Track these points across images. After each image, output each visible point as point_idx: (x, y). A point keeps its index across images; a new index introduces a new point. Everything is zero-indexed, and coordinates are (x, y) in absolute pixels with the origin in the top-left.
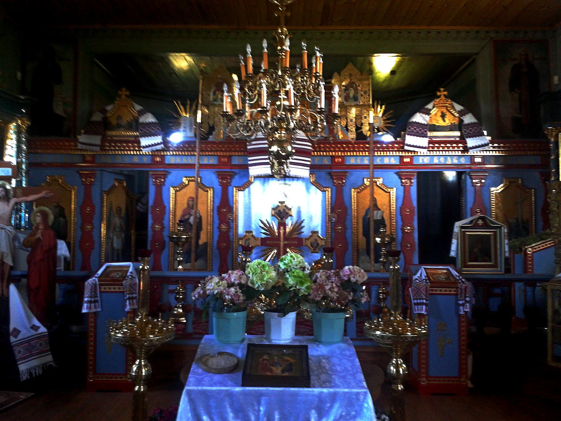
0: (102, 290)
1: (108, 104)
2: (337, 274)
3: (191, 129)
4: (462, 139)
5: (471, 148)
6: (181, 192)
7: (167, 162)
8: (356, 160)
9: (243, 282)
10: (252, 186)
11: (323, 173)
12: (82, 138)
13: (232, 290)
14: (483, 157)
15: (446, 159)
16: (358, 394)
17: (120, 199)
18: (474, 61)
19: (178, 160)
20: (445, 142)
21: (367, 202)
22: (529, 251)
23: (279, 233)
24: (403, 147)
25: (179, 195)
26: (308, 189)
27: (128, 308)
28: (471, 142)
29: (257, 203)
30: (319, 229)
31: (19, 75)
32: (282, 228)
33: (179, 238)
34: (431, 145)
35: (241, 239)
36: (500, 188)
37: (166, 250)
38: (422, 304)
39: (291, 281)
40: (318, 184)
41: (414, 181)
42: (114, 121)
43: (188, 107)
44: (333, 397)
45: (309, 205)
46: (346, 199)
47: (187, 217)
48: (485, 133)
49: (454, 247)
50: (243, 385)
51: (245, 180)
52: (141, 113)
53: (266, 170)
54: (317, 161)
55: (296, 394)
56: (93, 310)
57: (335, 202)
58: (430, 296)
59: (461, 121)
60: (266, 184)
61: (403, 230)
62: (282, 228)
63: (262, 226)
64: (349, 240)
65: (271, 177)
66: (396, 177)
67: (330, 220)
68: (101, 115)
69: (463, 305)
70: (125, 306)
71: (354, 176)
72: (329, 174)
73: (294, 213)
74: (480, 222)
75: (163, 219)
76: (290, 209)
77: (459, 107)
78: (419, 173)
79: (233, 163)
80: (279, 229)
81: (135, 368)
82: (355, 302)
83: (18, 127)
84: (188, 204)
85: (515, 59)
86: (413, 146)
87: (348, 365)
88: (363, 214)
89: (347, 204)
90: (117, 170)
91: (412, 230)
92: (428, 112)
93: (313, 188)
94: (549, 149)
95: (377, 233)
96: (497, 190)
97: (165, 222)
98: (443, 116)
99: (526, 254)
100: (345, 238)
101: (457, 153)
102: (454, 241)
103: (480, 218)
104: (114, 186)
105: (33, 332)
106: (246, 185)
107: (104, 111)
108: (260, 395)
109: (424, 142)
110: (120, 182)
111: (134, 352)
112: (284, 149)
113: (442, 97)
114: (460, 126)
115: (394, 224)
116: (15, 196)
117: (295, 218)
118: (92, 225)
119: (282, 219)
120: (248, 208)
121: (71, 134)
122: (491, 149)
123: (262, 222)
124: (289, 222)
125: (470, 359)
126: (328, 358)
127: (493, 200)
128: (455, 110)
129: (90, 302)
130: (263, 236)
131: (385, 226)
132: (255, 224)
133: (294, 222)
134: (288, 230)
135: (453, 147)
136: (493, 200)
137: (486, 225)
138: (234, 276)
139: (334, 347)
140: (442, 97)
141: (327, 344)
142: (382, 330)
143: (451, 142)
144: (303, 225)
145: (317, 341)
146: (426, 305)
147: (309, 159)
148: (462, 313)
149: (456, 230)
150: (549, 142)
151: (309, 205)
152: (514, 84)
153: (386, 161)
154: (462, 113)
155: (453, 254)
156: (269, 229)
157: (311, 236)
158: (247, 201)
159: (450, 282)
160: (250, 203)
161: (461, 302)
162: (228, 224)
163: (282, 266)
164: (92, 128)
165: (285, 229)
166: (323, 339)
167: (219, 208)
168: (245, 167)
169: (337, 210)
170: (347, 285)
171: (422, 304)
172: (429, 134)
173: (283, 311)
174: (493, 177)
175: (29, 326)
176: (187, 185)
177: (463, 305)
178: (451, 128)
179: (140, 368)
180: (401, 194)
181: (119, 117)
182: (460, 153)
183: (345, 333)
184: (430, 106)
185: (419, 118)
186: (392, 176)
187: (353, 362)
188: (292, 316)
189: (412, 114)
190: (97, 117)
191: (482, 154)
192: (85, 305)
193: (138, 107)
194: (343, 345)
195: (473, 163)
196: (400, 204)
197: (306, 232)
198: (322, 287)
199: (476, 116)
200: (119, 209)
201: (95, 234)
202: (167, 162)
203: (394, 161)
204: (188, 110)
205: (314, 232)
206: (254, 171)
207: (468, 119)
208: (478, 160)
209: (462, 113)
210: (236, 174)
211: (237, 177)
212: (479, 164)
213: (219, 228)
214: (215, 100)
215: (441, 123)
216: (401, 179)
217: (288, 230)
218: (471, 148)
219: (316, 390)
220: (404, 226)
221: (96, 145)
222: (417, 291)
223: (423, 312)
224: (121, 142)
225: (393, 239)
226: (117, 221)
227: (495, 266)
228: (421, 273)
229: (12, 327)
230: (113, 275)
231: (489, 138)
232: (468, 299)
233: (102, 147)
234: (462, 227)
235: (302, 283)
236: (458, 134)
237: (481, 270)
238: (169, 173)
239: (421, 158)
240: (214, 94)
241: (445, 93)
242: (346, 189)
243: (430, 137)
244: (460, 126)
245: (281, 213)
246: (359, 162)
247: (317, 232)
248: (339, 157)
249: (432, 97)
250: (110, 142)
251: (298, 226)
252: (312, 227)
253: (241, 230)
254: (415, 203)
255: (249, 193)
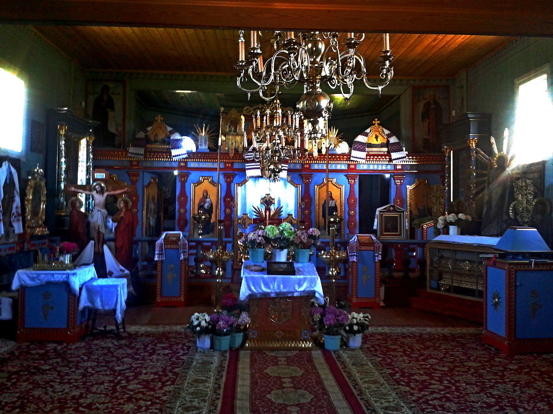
0: (166, 247)
1: (148, 126)
2: (307, 232)
3: (205, 144)
4: (389, 153)
5: (394, 160)
6: (199, 187)
7: (188, 166)
8: (318, 166)
9: (264, 235)
10: (247, 183)
11: (296, 175)
12: (131, 150)
13: (260, 238)
14: (402, 165)
15: (378, 167)
16: (314, 278)
17: (153, 191)
18: (399, 97)
19: (196, 165)
20: (378, 155)
21: (324, 195)
22: (425, 226)
23: (266, 215)
24: (350, 158)
25: (201, 189)
26: (285, 185)
27: (182, 257)
28: (394, 155)
29: (251, 194)
30: (293, 213)
31: (83, 103)
32: (268, 212)
33: (201, 218)
34: (368, 157)
35: (240, 219)
36: (413, 186)
37: (188, 227)
38: (354, 255)
39: (286, 234)
40: (292, 182)
41: (357, 181)
42: (152, 139)
43: (210, 131)
44: (305, 279)
45: (286, 195)
46: (311, 192)
47: (202, 204)
48: (404, 148)
49: (375, 223)
50: (268, 274)
51: (243, 179)
52: (172, 133)
53: (258, 173)
54: (292, 166)
55: (288, 278)
56: (161, 259)
57: (304, 194)
58: (358, 251)
59: (388, 141)
60: (257, 181)
61: (349, 214)
62: (268, 212)
63: (254, 210)
64: (313, 220)
65: (262, 177)
66: (345, 178)
67: (300, 206)
68: (144, 134)
69: (377, 256)
70: (179, 256)
71: (318, 178)
72: (300, 175)
73: (276, 202)
74: (392, 208)
75: (186, 204)
76: (274, 199)
77: (387, 132)
78: (360, 175)
79: (234, 167)
80: (266, 212)
81: (217, 272)
82: (315, 244)
83: (88, 142)
84: (203, 195)
85: (427, 99)
86: (356, 158)
87: (311, 269)
88: (322, 202)
89: (312, 196)
90: (151, 171)
91: (355, 213)
92: (366, 135)
93: (289, 185)
94: (444, 160)
95: (331, 215)
96: (409, 187)
97: (188, 207)
98: (377, 137)
99: (423, 228)
100: (310, 219)
101: (385, 163)
102: (376, 220)
103: (392, 206)
104: (150, 182)
105: (122, 273)
106: (243, 183)
107: (146, 131)
108: (275, 279)
109: (363, 155)
110: (154, 180)
111: (217, 265)
112: (277, 168)
113: (376, 124)
114: (387, 145)
115: (343, 211)
116: (107, 191)
117: (276, 206)
118: (137, 209)
119: (268, 205)
120: (244, 198)
121: (123, 146)
122: (408, 160)
123: (254, 208)
124: (272, 208)
125: (382, 289)
126: (302, 268)
127: (408, 193)
128: (384, 133)
129: (159, 254)
130: (255, 217)
131: (336, 211)
132: (249, 209)
133: (276, 208)
134: (272, 213)
135: (383, 159)
136: (408, 193)
137: (395, 211)
138: (260, 232)
139: (305, 264)
140: (376, 124)
141: (301, 263)
142: (326, 255)
143: (381, 155)
144: (282, 210)
145: (298, 262)
146: (356, 256)
147: (287, 166)
148: (377, 260)
149: (377, 213)
150: (445, 156)
151: (286, 195)
152: (425, 115)
153: (339, 167)
154: (389, 136)
155: (375, 227)
156: (259, 212)
157: (287, 218)
158: (244, 193)
159: (371, 243)
160: (245, 194)
161: (376, 255)
162: (231, 209)
163: (281, 228)
164: (137, 143)
165: (270, 212)
166: (300, 261)
167: (225, 198)
168: (244, 170)
169: (305, 200)
170: (311, 237)
171: (354, 255)
172: (367, 149)
173: (282, 249)
174: (409, 178)
175: (119, 270)
176: (202, 183)
177: (377, 256)
178: (382, 146)
179: (219, 271)
180: (348, 189)
181: (156, 135)
182: (387, 163)
183: (310, 260)
184: (368, 131)
185: (361, 139)
186: (343, 178)
187: (313, 269)
188: (285, 251)
189: (356, 136)
190: (141, 135)
191: (401, 163)
192: (156, 256)
193: (169, 129)
194: (308, 264)
195: (395, 169)
196: (347, 197)
197: (284, 214)
198: (300, 237)
199: (398, 138)
200: (153, 198)
201: (139, 215)
202: (188, 166)
203: (344, 167)
204: (212, 135)
205: (290, 215)
206: (249, 173)
207: (393, 140)
208: (399, 167)
209: (389, 136)
210: (236, 175)
211: (237, 177)
212: (400, 170)
213: (225, 211)
214: (230, 131)
215: (374, 142)
216: (349, 180)
217: (272, 213)
218: (394, 160)
219: (298, 277)
220: (349, 211)
221: (140, 155)
222: (352, 249)
223: (355, 260)
224: (158, 152)
225: (341, 219)
226: (152, 206)
227: (400, 235)
228: (355, 238)
229: (108, 271)
230: (171, 238)
231: (407, 153)
232: (380, 253)
233: (145, 156)
234: (380, 212)
235: (291, 235)
236: (385, 149)
237: (390, 238)
238: (190, 174)
239: (362, 165)
240: (229, 127)
241: (378, 122)
242: (311, 186)
243: (367, 152)
244: (387, 145)
245: (267, 201)
246: (320, 167)
247: (292, 215)
248: (307, 164)
249: (370, 125)
250: (151, 152)
251: (279, 211)
252: (288, 212)
253: (239, 213)
254: (357, 196)
255: (245, 187)
